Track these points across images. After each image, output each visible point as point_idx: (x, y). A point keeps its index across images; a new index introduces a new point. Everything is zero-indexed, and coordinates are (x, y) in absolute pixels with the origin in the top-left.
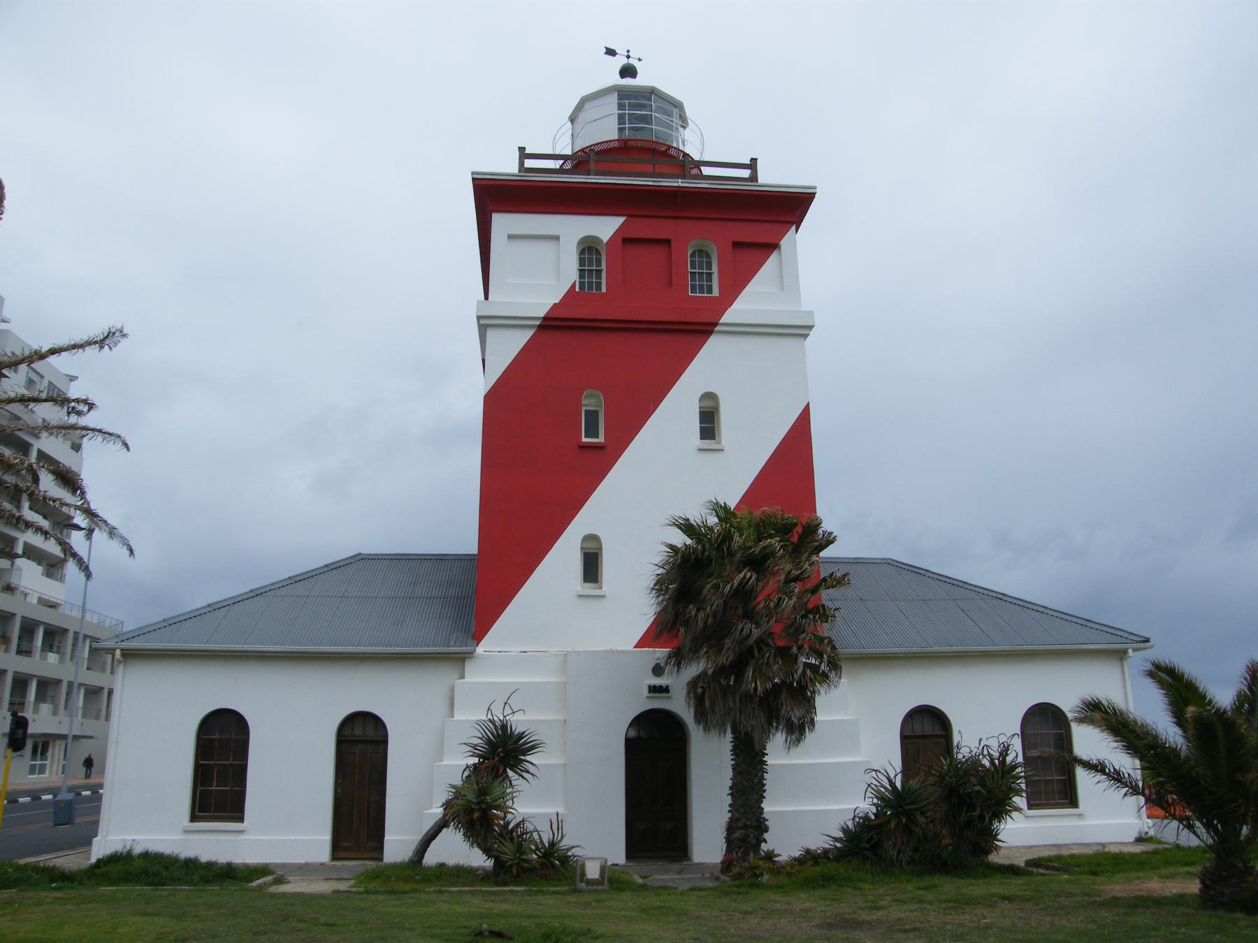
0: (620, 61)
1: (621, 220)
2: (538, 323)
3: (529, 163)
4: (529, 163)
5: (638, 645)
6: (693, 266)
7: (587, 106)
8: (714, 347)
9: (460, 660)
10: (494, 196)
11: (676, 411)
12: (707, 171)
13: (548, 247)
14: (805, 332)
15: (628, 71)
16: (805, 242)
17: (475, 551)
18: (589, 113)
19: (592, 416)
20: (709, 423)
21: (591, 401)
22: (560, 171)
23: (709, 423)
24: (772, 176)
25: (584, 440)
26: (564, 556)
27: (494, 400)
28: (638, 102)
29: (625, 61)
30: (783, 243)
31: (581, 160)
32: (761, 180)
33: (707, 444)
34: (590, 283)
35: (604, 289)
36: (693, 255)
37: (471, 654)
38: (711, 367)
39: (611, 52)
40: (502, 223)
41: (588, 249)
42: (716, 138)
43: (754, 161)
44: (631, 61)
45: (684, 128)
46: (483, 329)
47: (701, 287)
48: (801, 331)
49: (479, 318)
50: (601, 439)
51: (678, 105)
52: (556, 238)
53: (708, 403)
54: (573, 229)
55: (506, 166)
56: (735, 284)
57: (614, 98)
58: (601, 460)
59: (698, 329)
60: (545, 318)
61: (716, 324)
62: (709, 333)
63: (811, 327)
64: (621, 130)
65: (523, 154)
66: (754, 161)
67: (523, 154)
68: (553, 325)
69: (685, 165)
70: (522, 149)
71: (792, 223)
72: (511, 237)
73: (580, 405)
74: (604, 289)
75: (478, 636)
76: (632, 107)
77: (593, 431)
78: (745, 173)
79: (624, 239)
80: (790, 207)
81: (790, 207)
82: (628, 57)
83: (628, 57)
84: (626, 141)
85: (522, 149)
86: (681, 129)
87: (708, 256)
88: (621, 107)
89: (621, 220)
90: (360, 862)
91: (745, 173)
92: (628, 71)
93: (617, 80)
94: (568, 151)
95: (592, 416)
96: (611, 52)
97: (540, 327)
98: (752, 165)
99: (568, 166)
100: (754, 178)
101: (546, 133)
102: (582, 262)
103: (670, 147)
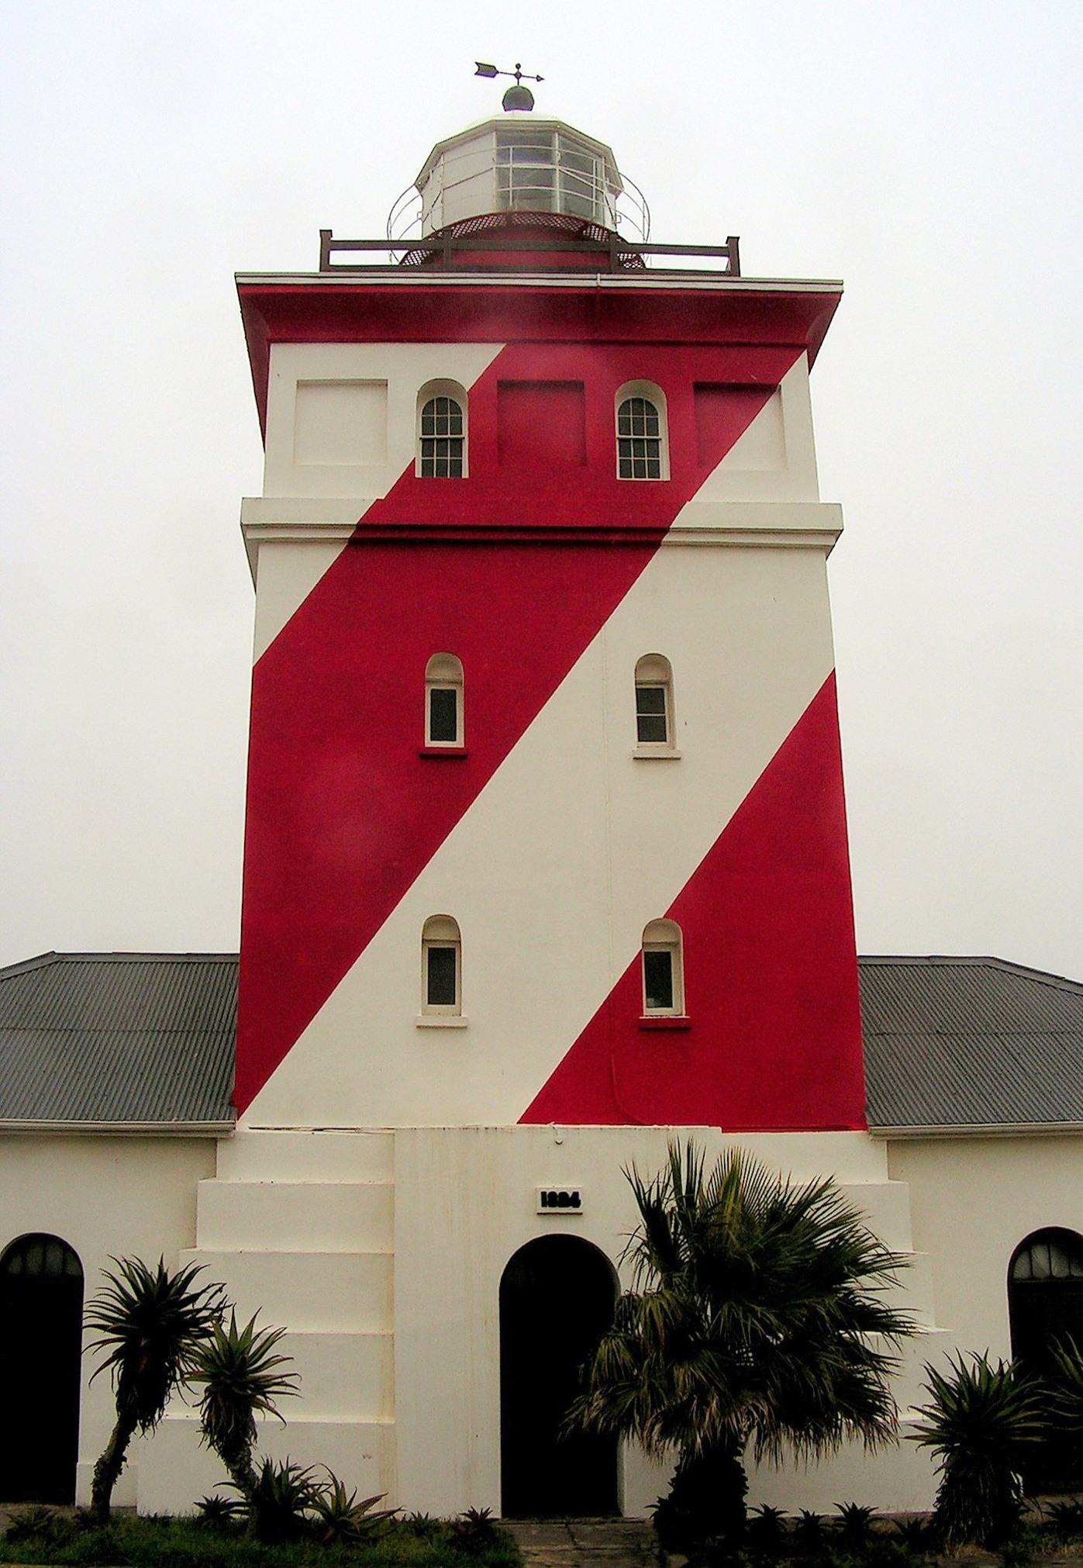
0: (504, 84)
1: (499, 348)
2: (348, 535)
3: (337, 258)
4: (337, 258)
5: (524, 1120)
6: (625, 427)
7: (448, 156)
8: (660, 571)
9: (211, 1141)
10: (278, 313)
11: (592, 691)
12: (653, 261)
13: (366, 400)
14: (829, 541)
15: (518, 99)
16: (831, 384)
17: (236, 949)
18: (452, 169)
19: (444, 701)
20: (652, 711)
21: (444, 673)
22: (401, 268)
23: (652, 711)
24: (765, 265)
25: (429, 743)
26: (392, 954)
27: (270, 677)
28: (528, 139)
29: (512, 82)
30: (785, 382)
31: (437, 249)
32: (745, 273)
33: (652, 748)
34: (442, 465)
35: (465, 474)
36: (624, 408)
37: (227, 1133)
38: (657, 610)
39: (487, 71)
40: (291, 361)
41: (437, 404)
42: (674, 209)
43: (733, 241)
44: (523, 82)
45: (616, 193)
46: (252, 549)
47: (639, 465)
48: (823, 539)
49: (244, 527)
50: (459, 743)
51: (604, 153)
52: (383, 384)
53: (652, 676)
54: (411, 367)
55: (296, 260)
56: (699, 460)
57: (491, 143)
58: (456, 783)
59: (630, 537)
60: (360, 527)
61: (665, 531)
62: (654, 546)
63: (837, 533)
64: (504, 197)
65: (328, 243)
66: (733, 241)
67: (328, 243)
68: (375, 538)
69: (610, 252)
70: (326, 234)
71: (801, 347)
72: (302, 385)
73: (423, 682)
74: (465, 474)
75: (240, 1101)
76: (520, 156)
77: (445, 731)
78: (720, 264)
79: (498, 385)
80: (779, 325)
81: (779, 325)
82: (518, 76)
83: (518, 76)
84: (508, 216)
85: (326, 234)
86: (610, 197)
87: (652, 410)
88: (503, 155)
89: (499, 348)
90: (244, 1181)
91: (720, 264)
92: (518, 99)
93: (495, 111)
94: (416, 234)
95: (444, 701)
96: (487, 71)
97: (352, 542)
98: (731, 249)
99: (416, 258)
100: (734, 269)
101: (372, 203)
102: (427, 425)
103: (587, 225)
